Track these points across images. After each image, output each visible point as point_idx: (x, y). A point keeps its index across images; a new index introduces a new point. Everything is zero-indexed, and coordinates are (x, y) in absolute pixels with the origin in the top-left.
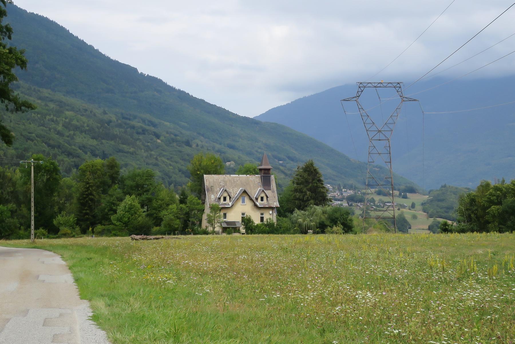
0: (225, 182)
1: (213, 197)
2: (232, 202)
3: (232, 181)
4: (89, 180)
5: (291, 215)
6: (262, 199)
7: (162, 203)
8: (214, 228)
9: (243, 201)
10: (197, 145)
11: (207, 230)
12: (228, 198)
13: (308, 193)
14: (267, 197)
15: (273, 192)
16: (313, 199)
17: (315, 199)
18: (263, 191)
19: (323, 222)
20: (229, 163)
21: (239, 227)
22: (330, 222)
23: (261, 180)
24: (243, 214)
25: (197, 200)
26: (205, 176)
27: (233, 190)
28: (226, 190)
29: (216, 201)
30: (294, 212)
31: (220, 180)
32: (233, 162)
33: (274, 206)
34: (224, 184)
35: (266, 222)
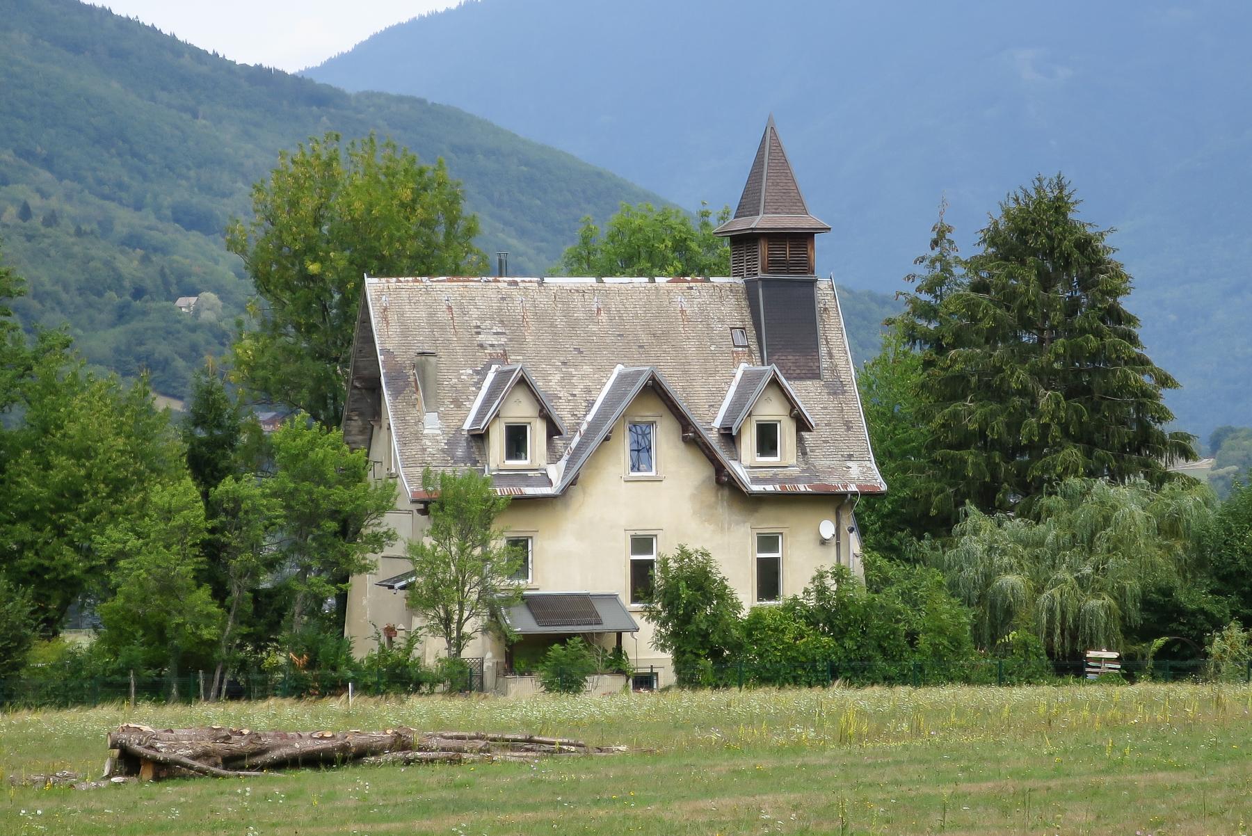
0: (511, 326)
1: (432, 425)
2: (562, 464)
3: (560, 322)
5: (934, 548)
6: (767, 440)
8: (458, 642)
9: (642, 453)
10: (26, 213)
11: (416, 653)
12: (537, 435)
13: (1042, 402)
14: (802, 425)
15: (836, 389)
16: (1076, 440)
17: (1087, 441)
18: (774, 382)
19: (1167, 592)
20: (193, 300)
21: (619, 636)
22: (1212, 592)
23: (747, 313)
24: (642, 543)
25: (337, 448)
26: (372, 285)
27: (566, 379)
28: (523, 382)
29: (460, 452)
30: (957, 529)
31: (475, 313)
32: (212, 295)
34: (503, 340)
35: (813, 595)
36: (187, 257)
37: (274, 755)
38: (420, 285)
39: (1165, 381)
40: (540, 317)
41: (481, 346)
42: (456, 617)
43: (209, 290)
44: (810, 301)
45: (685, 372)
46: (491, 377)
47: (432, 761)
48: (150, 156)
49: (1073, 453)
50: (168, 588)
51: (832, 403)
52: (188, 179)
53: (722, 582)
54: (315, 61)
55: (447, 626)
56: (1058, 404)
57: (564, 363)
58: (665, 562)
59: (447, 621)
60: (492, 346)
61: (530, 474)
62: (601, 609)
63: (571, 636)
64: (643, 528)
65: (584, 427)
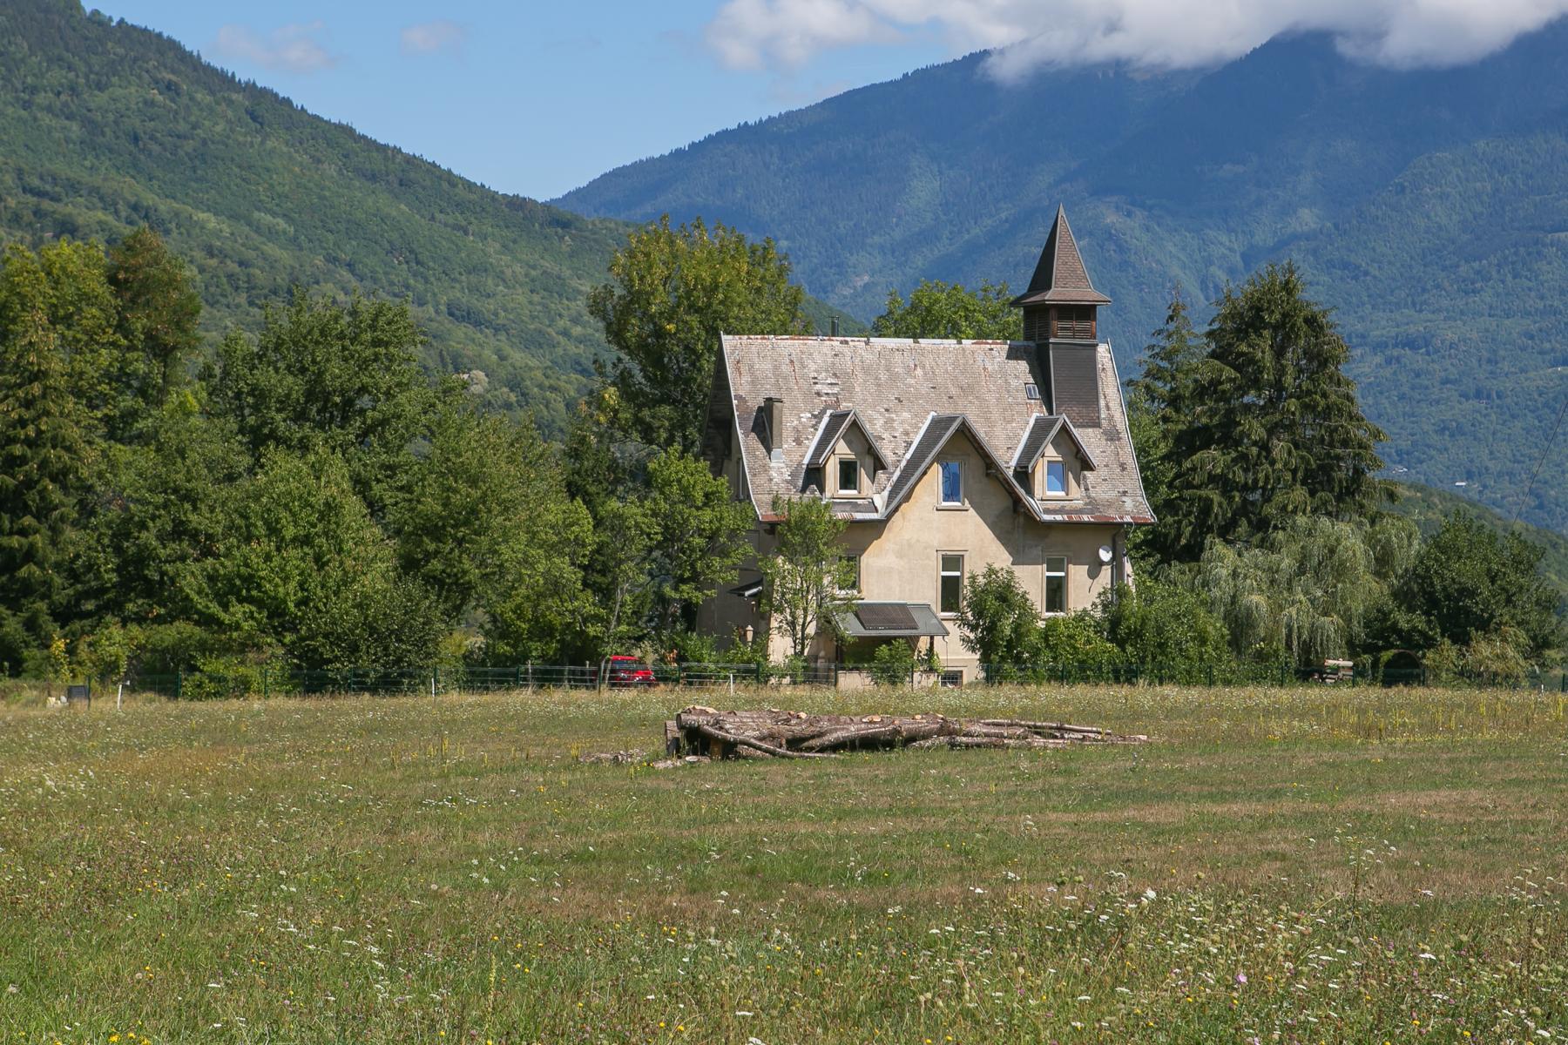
2: (886, 493)
3: (883, 377)
4: (45, 358)
7: (478, 494)
15: (1112, 436)
21: (932, 638)
24: (952, 561)
27: (889, 423)
31: (813, 367)
33: (1128, 519)
34: (836, 390)
36: (459, 343)
37: (831, 738)
38: (768, 342)
39: (1376, 435)
40: (867, 370)
41: (818, 394)
42: (801, 621)
43: (477, 368)
44: (1093, 361)
45: (987, 419)
46: (826, 420)
47: (978, 745)
48: (431, 264)
49: (1300, 493)
50: (556, 587)
51: (1110, 448)
52: (460, 282)
53: (1023, 597)
54: (559, 194)
55: (794, 629)
56: (1290, 453)
57: (887, 410)
58: (973, 578)
59: (793, 624)
60: (446, 225)
61: (860, 501)
62: (916, 615)
63: (895, 638)
64: (954, 548)
65: (904, 463)
